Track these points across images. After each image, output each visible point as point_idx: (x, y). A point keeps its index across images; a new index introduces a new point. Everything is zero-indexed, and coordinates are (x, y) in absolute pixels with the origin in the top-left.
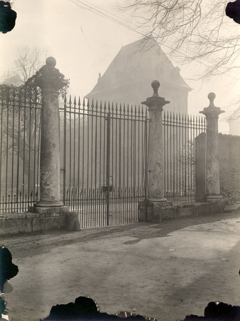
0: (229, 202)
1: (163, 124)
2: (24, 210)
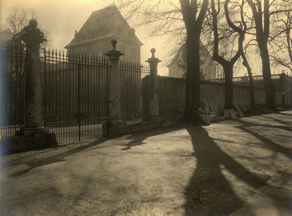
0: (165, 120)
1: (119, 69)
2: (12, 134)
